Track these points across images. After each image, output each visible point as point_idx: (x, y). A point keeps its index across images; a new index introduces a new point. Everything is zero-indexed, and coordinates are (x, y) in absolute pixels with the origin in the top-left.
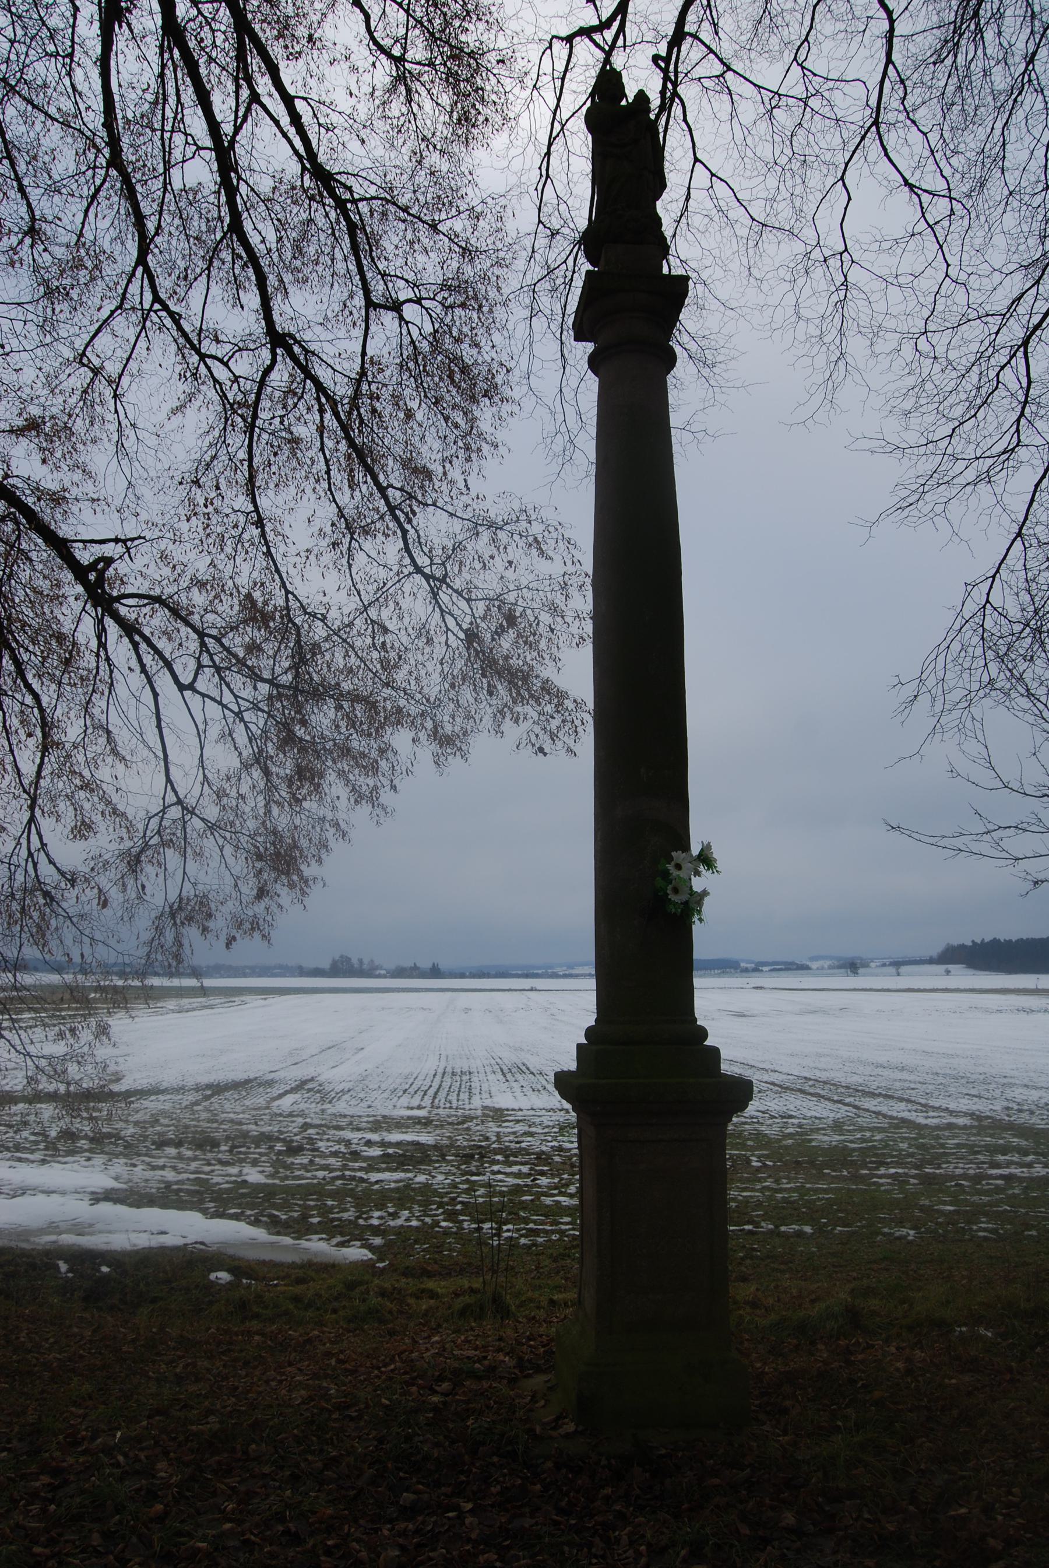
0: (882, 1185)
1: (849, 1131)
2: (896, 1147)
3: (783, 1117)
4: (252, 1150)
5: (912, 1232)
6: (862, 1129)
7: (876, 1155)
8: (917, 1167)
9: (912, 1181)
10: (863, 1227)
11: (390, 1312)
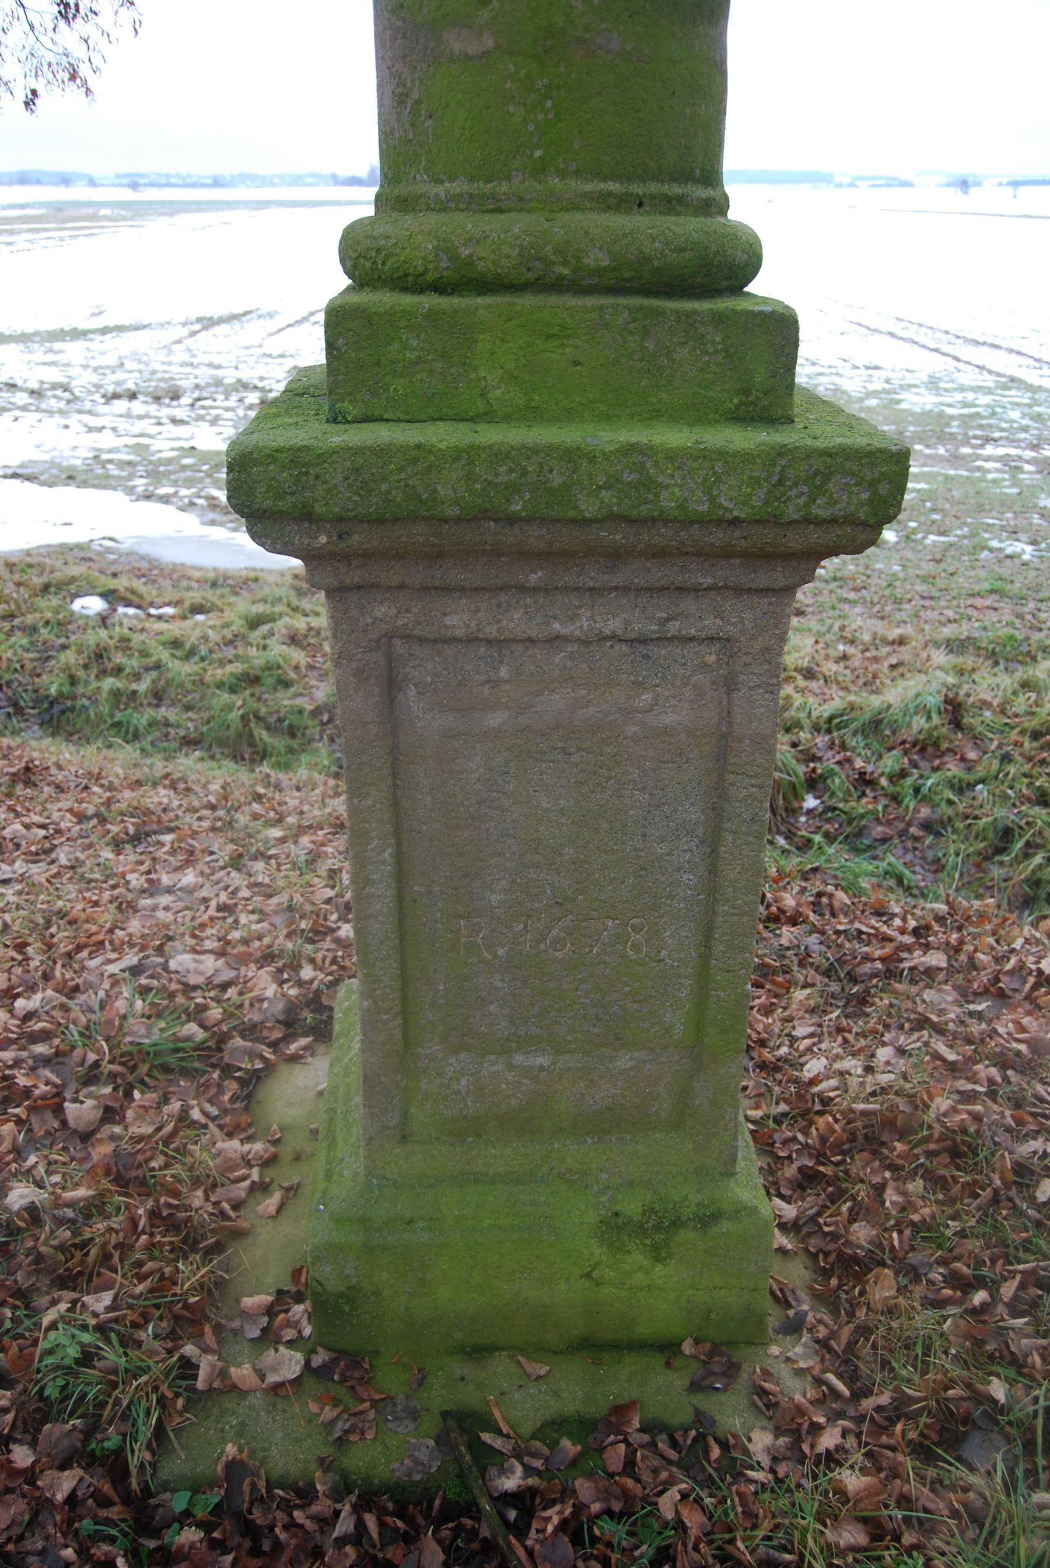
0: (989, 471)
1: (947, 390)
2: (1005, 416)
3: (867, 368)
4: (218, 403)
5: (1029, 549)
6: (962, 389)
7: (981, 427)
8: (1035, 447)
9: (1028, 467)
10: (965, 537)
11: (297, 668)
